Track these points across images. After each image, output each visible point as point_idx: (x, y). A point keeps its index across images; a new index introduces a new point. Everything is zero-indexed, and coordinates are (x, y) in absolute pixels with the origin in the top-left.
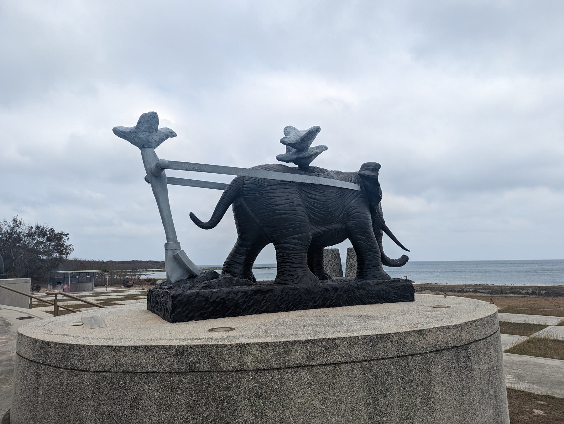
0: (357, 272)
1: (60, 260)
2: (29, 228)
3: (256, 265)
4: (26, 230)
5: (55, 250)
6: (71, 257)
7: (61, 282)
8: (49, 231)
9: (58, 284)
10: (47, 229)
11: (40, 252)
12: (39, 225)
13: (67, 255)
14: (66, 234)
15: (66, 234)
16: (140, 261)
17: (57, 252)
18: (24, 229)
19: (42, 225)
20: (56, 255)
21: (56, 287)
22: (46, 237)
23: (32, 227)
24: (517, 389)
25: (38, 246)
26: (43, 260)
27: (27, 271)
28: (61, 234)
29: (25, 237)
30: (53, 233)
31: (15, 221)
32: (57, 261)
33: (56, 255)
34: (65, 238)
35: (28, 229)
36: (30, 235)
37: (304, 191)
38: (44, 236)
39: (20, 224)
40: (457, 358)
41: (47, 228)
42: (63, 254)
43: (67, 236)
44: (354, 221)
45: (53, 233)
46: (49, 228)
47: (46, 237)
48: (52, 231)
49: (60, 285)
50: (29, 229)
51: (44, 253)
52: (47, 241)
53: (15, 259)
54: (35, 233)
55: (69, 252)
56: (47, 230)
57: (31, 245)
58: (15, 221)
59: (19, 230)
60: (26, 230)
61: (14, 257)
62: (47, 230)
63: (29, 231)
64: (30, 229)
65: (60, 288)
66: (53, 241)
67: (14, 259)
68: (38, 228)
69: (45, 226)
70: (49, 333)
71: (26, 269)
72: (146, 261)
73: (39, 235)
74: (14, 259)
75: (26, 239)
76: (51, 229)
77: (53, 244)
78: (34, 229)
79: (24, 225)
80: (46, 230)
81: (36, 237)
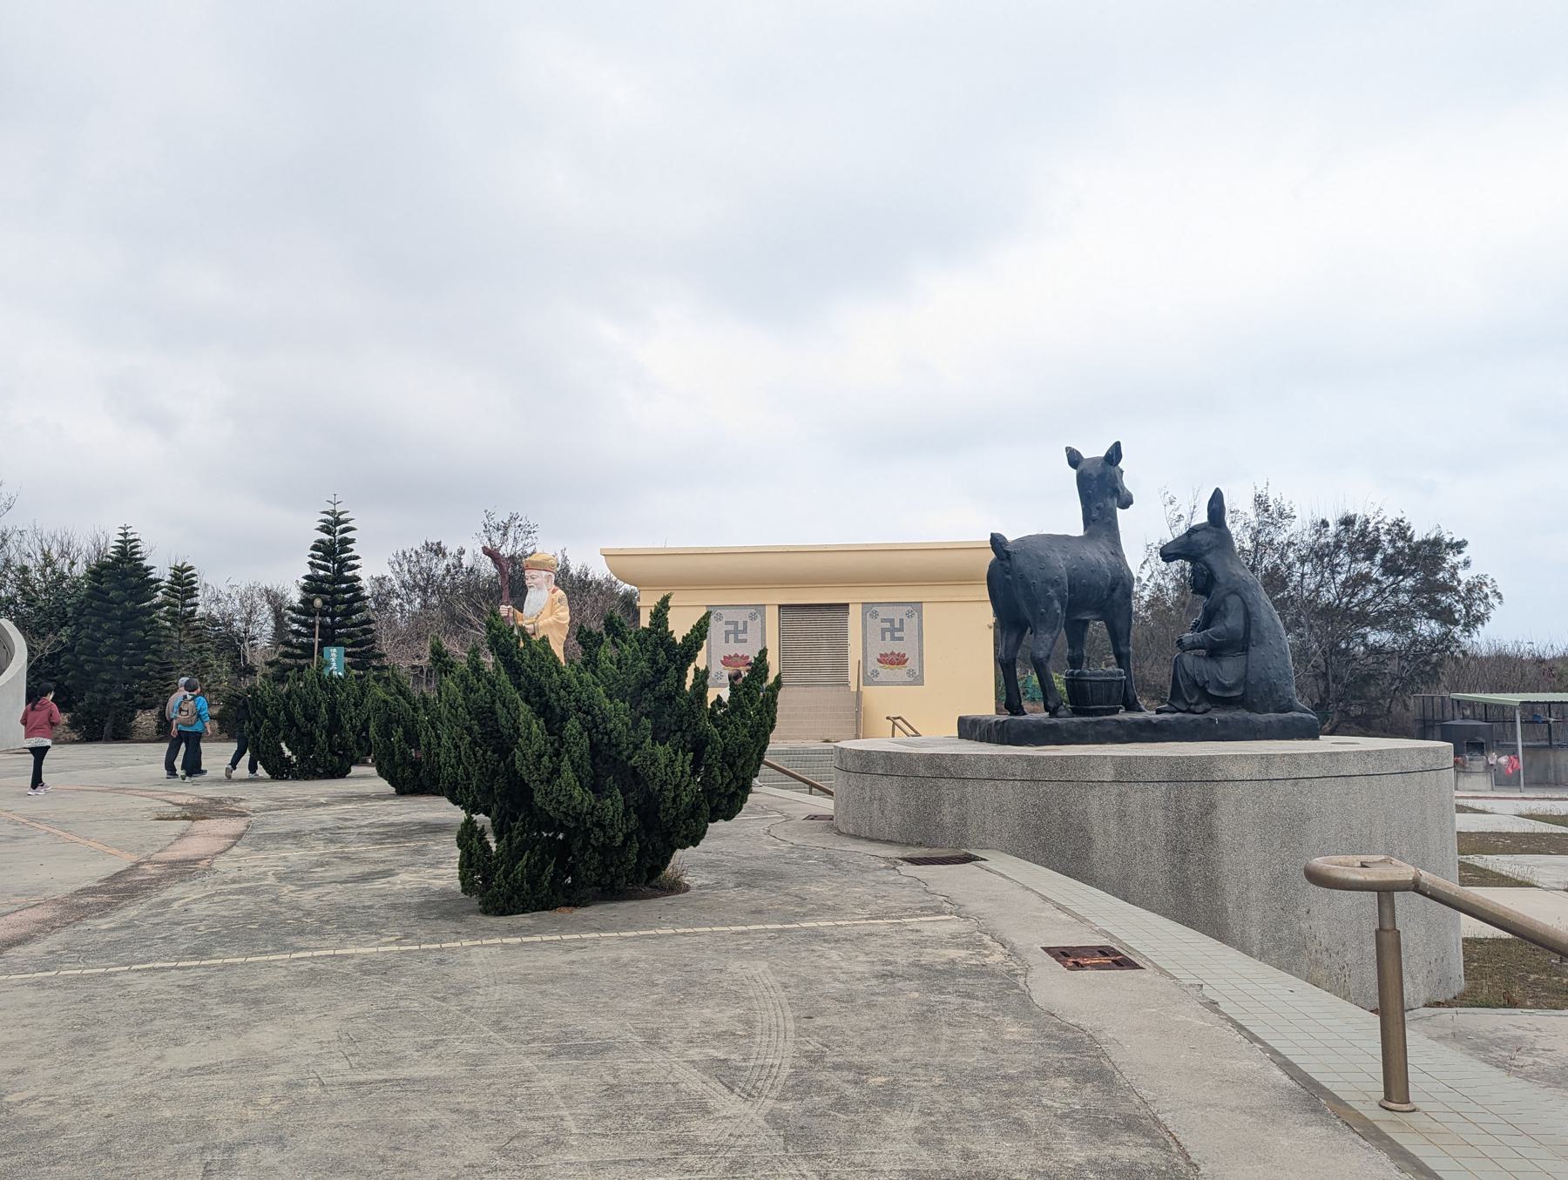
0: (1270, 722)
2: (1316, 524)
3: (221, 754)
4: (1306, 533)
5: (1422, 607)
6: (1485, 639)
7: (1481, 740)
8: (1388, 532)
9: (1468, 751)
10: (1379, 522)
11: (1362, 618)
12: (1351, 512)
13: (1468, 627)
14: (1454, 541)
15: (1458, 543)
18: (1298, 529)
19: (1360, 509)
20: (1427, 628)
22: (1379, 557)
23: (1325, 524)
24: (1467, 757)
25: (1354, 594)
27: (1322, 689)
28: (1437, 542)
29: (1303, 564)
30: (1404, 538)
31: (1261, 503)
33: (1427, 628)
34: (1452, 559)
35: (1313, 531)
36: (1321, 555)
37: (191, 1072)
38: (1370, 557)
41: (1380, 519)
42: (1456, 623)
43: (1460, 552)
44: (184, 898)
45: (1404, 538)
46: (1389, 521)
47: (1379, 557)
48: (1400, 531)
49: (1477, 755)
50: (1317, 531)
52: (1383, 575)
54: (1338, 546)
56: (1380, 526)
57: (1328, 596)
60: (1306, 533)
62: (1380, 526)
63: (1315, 537)
64: (1320, 530)
65: (1482, 769)
66: (1407, 574)
68: (1348, 522)
69: (1370, 515)
70: (1423, 901)
73: (1352, 551)
75: (1308, 568)
76: (1397, 523)
78: (1332, 529)
79: (1295, 517)
81: (1342, 557)
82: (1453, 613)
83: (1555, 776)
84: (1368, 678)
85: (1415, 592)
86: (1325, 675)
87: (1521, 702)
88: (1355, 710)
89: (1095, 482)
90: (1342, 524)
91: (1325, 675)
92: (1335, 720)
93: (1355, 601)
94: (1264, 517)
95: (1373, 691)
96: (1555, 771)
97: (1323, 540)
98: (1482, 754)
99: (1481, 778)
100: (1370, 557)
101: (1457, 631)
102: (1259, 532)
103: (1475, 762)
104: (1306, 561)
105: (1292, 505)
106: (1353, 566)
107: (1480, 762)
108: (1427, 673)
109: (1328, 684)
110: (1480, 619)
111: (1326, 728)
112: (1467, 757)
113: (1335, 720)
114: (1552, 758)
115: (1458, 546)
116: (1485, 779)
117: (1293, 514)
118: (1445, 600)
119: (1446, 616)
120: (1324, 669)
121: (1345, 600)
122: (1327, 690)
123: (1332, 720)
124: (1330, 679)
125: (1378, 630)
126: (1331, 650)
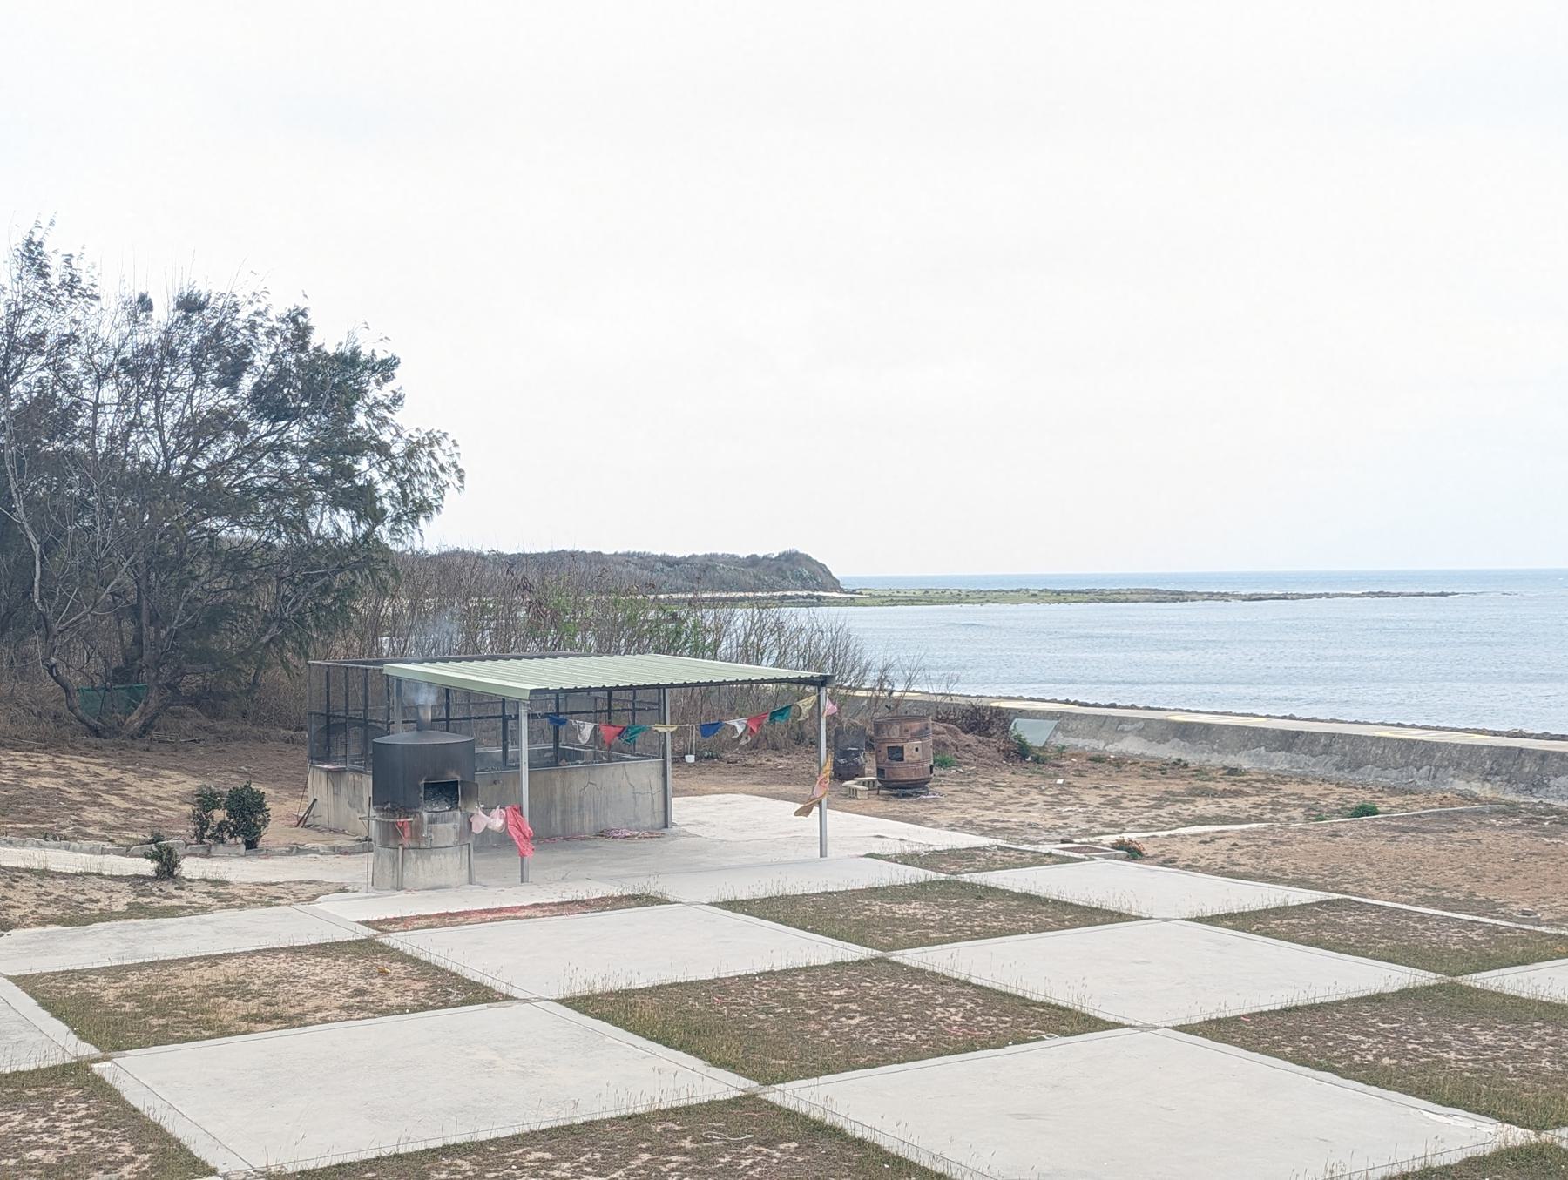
1: (367, 554)
7: (453, 775)
10: (258, 313)
14: (379, 358)
15: (383, 362)
16: (594, 553)
17: (335, 505)
19: (211, 283)
21: (416, 831)
23: (145, 303)
25: (196, 453)
26: (236, 560)
27: (128, 639)
31: (33, 257)
32: (341, 569)
34: (377, 392)
39: (71, 284)
40: (686, 693)
49: (441, 807)
51: (239, 506)
53: (47, 548)
55: (430, 493)
58: (33, 257)
59: (55, 325)
61: (40, 533)
65: (452, 839)
66: (292, 415)
67: (37, 549)
68: (190, 305)
71: (126, 625)
72: (613, 552)
74: (37, 549)
77: (297, 432)
79: (98, 298)
80: (253, 326)
82: (374, 500)
83: (563, 820)
84: (217, 616)
85: (312, 453)
86: (136, 610)
87: (533, 692)
88: (192, 682)
89: (348, 485)
90: (179, 306)
91: (136, 610)
92: (152, 704)
93: (202, 463)
94: (35, 286)
95: (229, 642)
96: (564, 812)
97: (142, 338)
98: (454, 806)
99: (449, 858)
100: (230, 378)
101: (383, 532)
102: (21, 313)
103: (439, 826)
104: (106, 376)
105: (94, 273)
106: (197, 393)
107: (450, 825)
108: (327, 608)
109: (141, 628)
110: (423, 508)
111: (132, 723)
112: (425, 815)
113: (152, 704)
114: (558, 785)
115: (386, 368)
116: (457, 860)
117: (96, 291)
118: (365, 468)
119: (362, 501)
120: (133, 596)
121: (181, 460)
122: (138, 641)
123: (146, 704)
124: (144, 620)
125: (240, 524)
126: (148, 562)
